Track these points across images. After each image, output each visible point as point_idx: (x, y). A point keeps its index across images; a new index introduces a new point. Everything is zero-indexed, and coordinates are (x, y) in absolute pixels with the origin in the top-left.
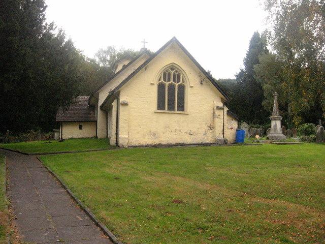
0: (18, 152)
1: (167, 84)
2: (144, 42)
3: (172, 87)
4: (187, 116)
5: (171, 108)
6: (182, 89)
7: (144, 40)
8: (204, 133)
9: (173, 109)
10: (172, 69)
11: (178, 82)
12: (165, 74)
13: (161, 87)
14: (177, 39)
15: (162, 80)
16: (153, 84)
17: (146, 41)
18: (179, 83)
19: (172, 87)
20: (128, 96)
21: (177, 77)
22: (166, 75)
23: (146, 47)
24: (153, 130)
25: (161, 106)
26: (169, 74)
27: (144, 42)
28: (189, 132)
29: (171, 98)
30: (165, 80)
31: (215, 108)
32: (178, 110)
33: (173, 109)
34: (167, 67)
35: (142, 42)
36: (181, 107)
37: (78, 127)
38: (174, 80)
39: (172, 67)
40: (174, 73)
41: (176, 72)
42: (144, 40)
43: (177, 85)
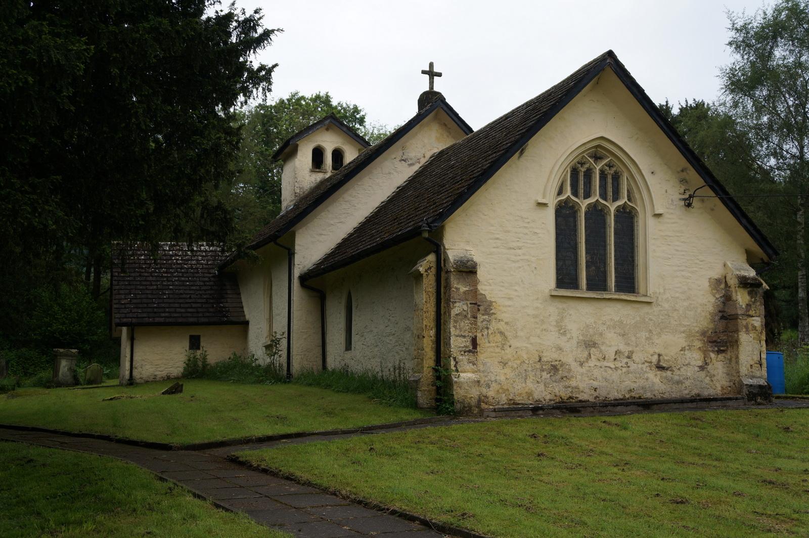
0: (302, 523)
1: (584, 204)
2: (431, 73)
3: (596, 214)
4: (646, 309)
5: (597, 283)
6: (627, 219)
7: (431, 65)
8: (700, 363)
9: (603, 287)
10: (597, 158)
11: (616, 197)
12: (575, 172)
13: (565, 215)
14: (621, 58)
15: (568, 193)
16: (545, 205)
17: (436, 70)
18: (620, 203)
19: (596, 214)
20: (468, 242)
21: (613, 182)
22: (578, 176)
23: (436, 89)
24: (550, 356)
25: (566, 278)
26: (589, 174)
27: (431, 73)
28: (655, 359)
29: (596, 252)
30: (575, 192)
31: (733, 282)
32: (590, 287)
33: (603, 287)
34: (583, 149)
35: (424, 72)
36: (628, 282)
37: (186, 344)
38: (604, 195)
39: (598, 150)
40: (602, 172)
41: (610, 166)
42: (431, 65)
43: (613, 207)
